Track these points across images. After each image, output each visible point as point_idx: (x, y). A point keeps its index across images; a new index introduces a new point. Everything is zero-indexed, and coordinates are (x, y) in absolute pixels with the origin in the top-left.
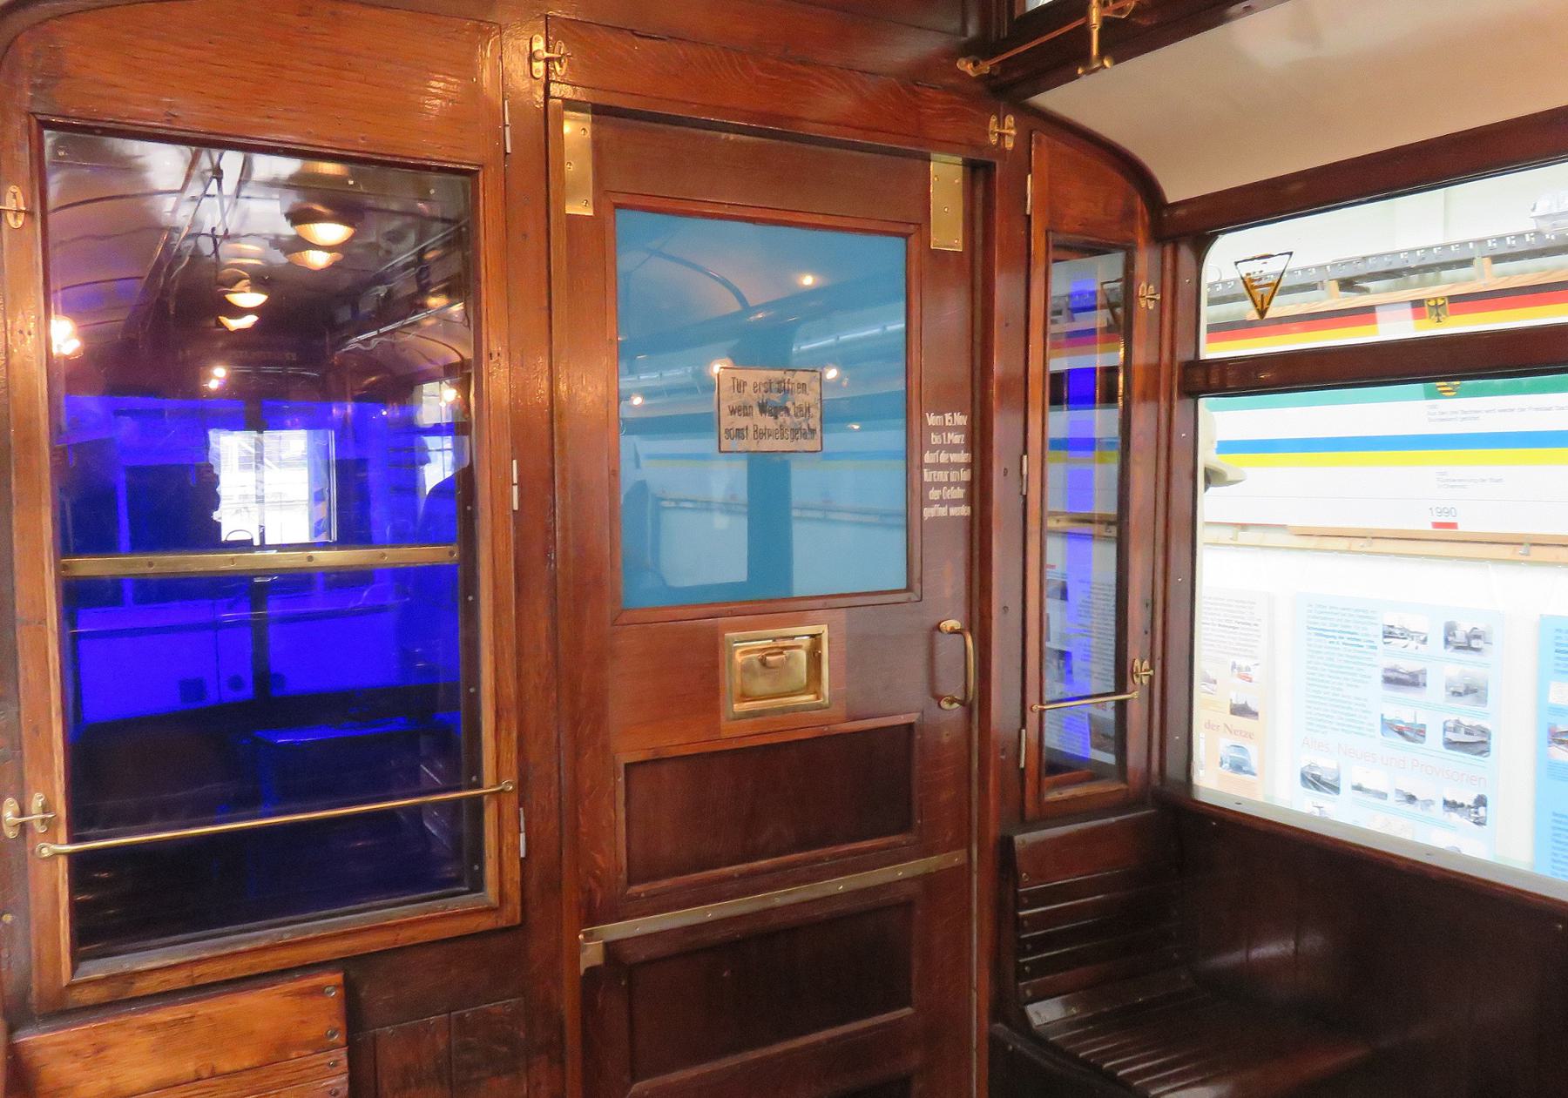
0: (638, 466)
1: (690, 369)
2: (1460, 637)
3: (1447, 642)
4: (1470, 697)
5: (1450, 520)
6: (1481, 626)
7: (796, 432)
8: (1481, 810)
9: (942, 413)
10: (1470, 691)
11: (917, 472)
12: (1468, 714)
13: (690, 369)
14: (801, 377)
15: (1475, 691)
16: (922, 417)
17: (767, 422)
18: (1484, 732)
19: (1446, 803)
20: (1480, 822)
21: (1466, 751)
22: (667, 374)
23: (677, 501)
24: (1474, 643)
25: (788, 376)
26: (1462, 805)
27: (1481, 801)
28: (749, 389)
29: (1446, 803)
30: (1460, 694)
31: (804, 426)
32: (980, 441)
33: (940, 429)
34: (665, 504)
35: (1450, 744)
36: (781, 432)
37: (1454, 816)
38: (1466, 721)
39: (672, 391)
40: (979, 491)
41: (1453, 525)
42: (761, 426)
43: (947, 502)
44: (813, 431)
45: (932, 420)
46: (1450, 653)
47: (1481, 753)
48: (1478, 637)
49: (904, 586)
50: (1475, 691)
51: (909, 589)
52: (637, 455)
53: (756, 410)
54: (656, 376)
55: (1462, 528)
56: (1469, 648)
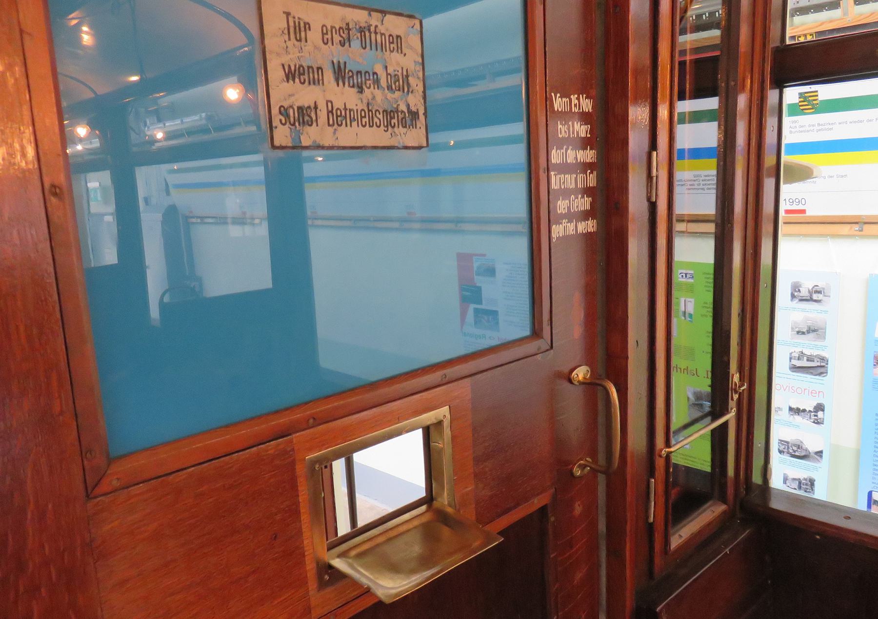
0: (168, 193)
1: (204, 115)
2: (804, 293)
3: (793, 296)
4: (811, 335)
5: (800, 207)
6: (821, 285)
7: (392, 117)
8: (820, 414)
9: (568, 96)
10: (812, 331)
11: (543, 176)
12: (810, 347)
13: (204, 115)
14: (393, 25)
15: (814, 331)
16: (548, 100)
17: (346, 97)
18: (823, 359)
19: (791, 409)
20: (818, 422)
21: (803, 372)
22: (186, 120)
23: (202, 218)
24: (815, 297)
25: (375, 20)
26: (804, 411)
27: (820, 408)
28: (314, 36)
29: (791, 409)
30: (803, 333)
31: (403, 107)
32: (607, 134)
33: (565, 116)
34: (194, 220)
35: (795, 368)
36: (367, 116)
37: (798, 419)
38: (807, 352)
39: (190, 132)
40: (608, 200)
41: (803, 211)
42: (338, 104)
43: (571, 221)
44: (414, 115)
45: (559, 103)
46: (796, 304)
47: (820, 374)
48: (819, 292)
49: (527, 332)
50: (814, 331)
51: (536, 333)
52: (167, 184)
53: (329, 76)
54: (178, 122)
55: (808, 214)
56: (811, 300)
